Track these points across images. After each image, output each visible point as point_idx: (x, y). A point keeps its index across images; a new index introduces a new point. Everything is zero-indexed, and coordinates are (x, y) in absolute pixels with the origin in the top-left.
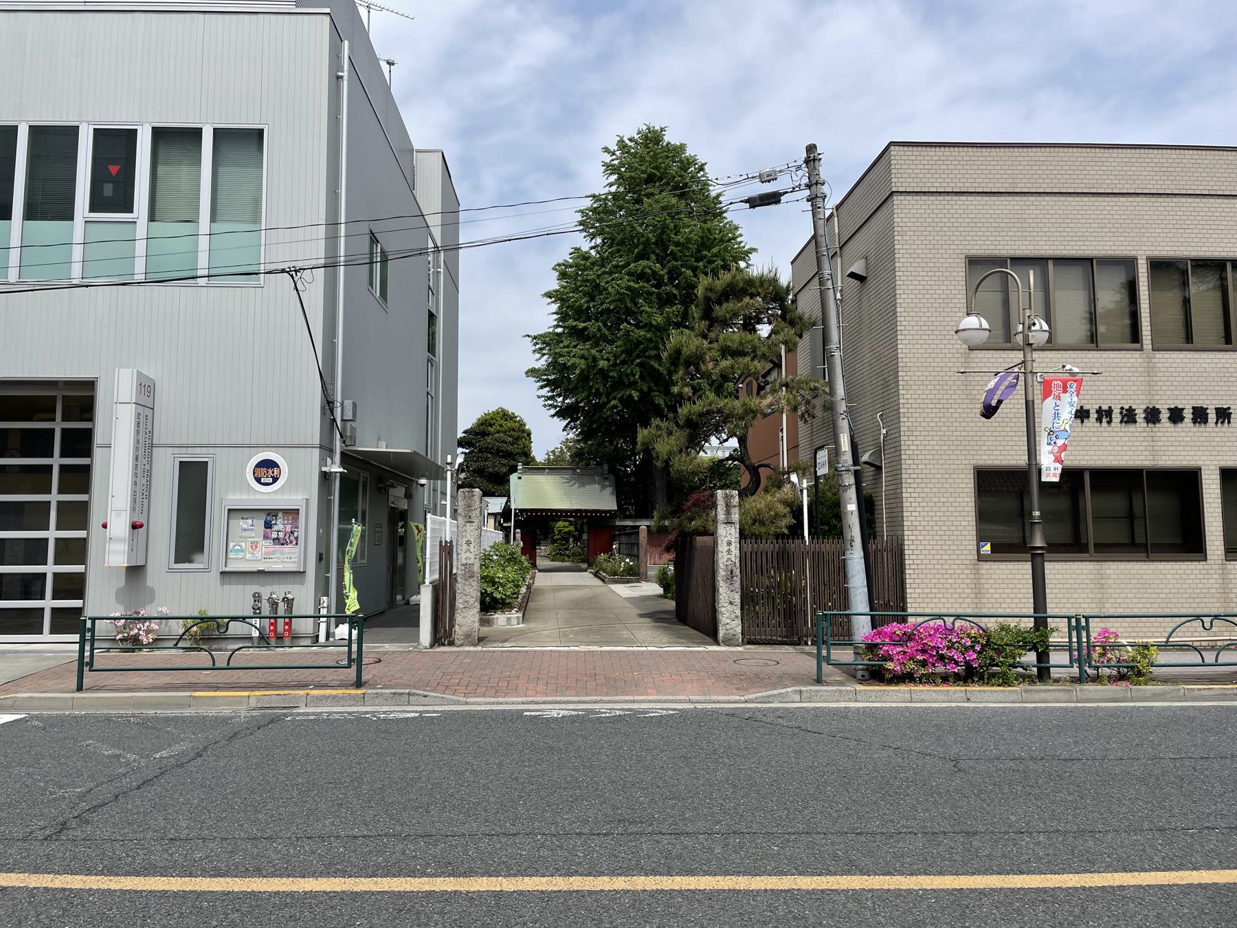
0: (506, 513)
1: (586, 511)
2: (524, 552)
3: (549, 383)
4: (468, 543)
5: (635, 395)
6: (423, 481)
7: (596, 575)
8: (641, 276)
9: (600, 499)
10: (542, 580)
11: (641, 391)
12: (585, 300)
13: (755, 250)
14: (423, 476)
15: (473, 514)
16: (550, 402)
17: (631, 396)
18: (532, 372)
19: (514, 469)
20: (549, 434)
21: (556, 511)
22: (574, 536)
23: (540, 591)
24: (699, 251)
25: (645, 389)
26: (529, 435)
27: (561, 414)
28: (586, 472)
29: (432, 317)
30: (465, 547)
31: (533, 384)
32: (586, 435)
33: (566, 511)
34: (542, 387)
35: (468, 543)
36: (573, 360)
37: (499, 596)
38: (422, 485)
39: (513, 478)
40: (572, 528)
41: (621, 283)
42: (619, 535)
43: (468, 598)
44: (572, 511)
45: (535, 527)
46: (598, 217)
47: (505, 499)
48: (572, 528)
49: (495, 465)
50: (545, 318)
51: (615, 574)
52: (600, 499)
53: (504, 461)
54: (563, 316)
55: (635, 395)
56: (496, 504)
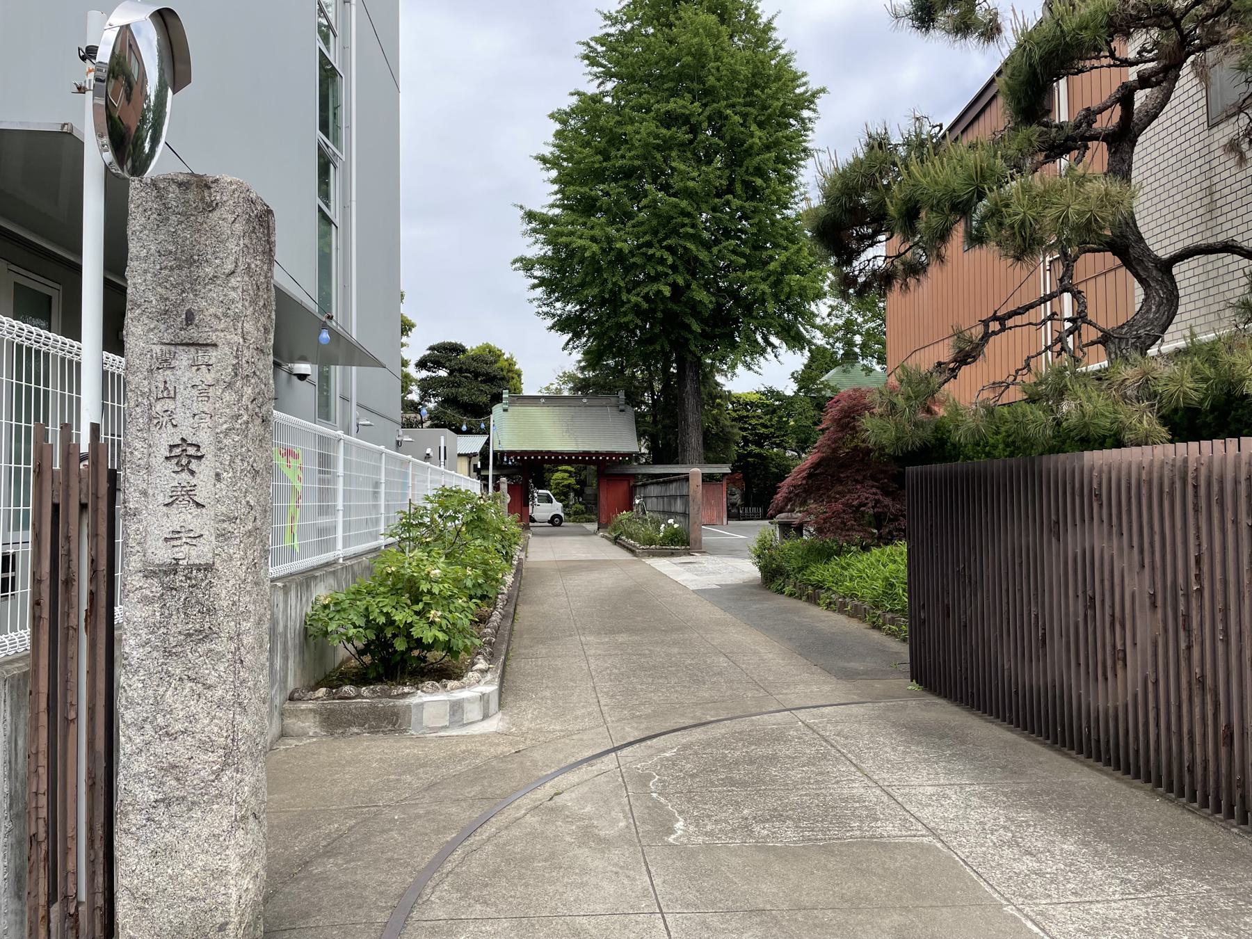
0: (484, 454)
1: (597, 454)
2: (511, 509)
3: (543, 282)
4: (184, 455)
5: (667, 291)
6: (303, 368)
7: (616, 541)
8: (669, 120)
9: (613, 434)
10: (543, 551)
11: (674, 286)
12: (595, 158)
13: (823, 90)
14: (303, 359)
15: (208, 305)
16: (545, 309)
17: (659, 292)
18: (527, 265)
19: (497, 398)
20: (545, 357)
21: (556, 453)
22: (575, 491)
23: (540, 574)
24: (749, 93)
25: (680, 281)
26: (519, 376)
27: (563, 324)
28: (595, 402)
29: (328, 75)
30: (166, 477)
31: (522, 281)
32: (593, 359)
33: (570, 454)
34: (534, 287)
35: (184, 455)
36: (580, 242)
37: (428, 635)
38: (302, 377)
39: (497, 409)
40: (572, 481)
41: (645, 129)
42: (644, 485)
43: (180, 750)
44: (577, 454)
45: (524, 473)
46: (613, 54)
47: (486, 437)
48: (572, 481)
49: (469, 392)
50: (543, 193)
51: (651, 541)
52: (613, 434)
53: (484, 387)
54: (564, 181)
55: (667, 291)
56: (473, 444)
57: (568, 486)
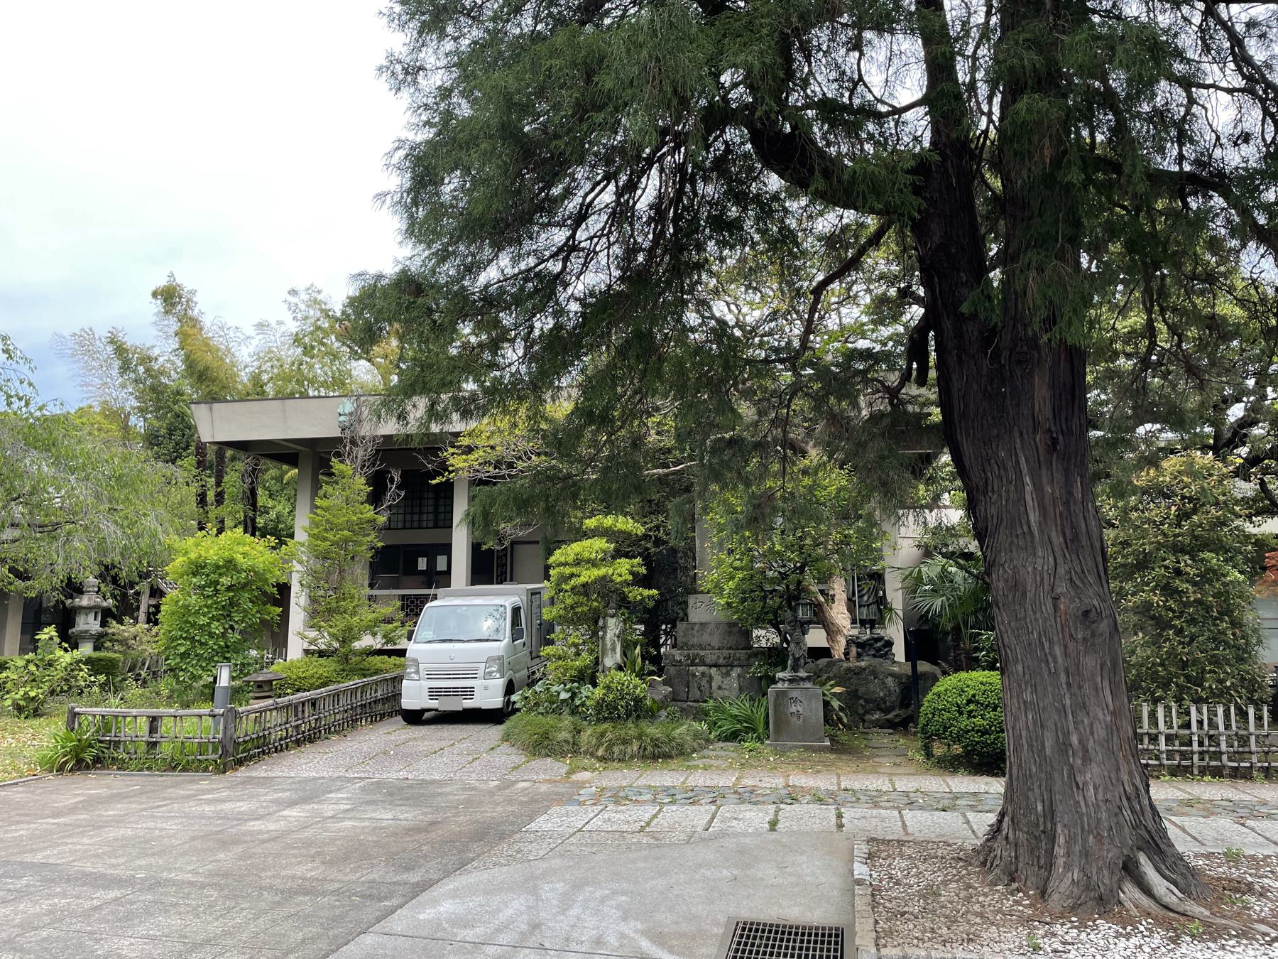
57: (604, 588)
